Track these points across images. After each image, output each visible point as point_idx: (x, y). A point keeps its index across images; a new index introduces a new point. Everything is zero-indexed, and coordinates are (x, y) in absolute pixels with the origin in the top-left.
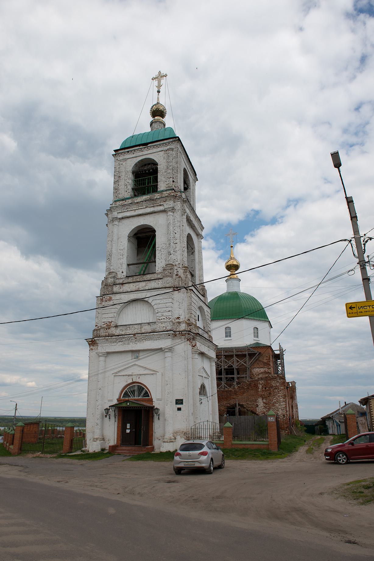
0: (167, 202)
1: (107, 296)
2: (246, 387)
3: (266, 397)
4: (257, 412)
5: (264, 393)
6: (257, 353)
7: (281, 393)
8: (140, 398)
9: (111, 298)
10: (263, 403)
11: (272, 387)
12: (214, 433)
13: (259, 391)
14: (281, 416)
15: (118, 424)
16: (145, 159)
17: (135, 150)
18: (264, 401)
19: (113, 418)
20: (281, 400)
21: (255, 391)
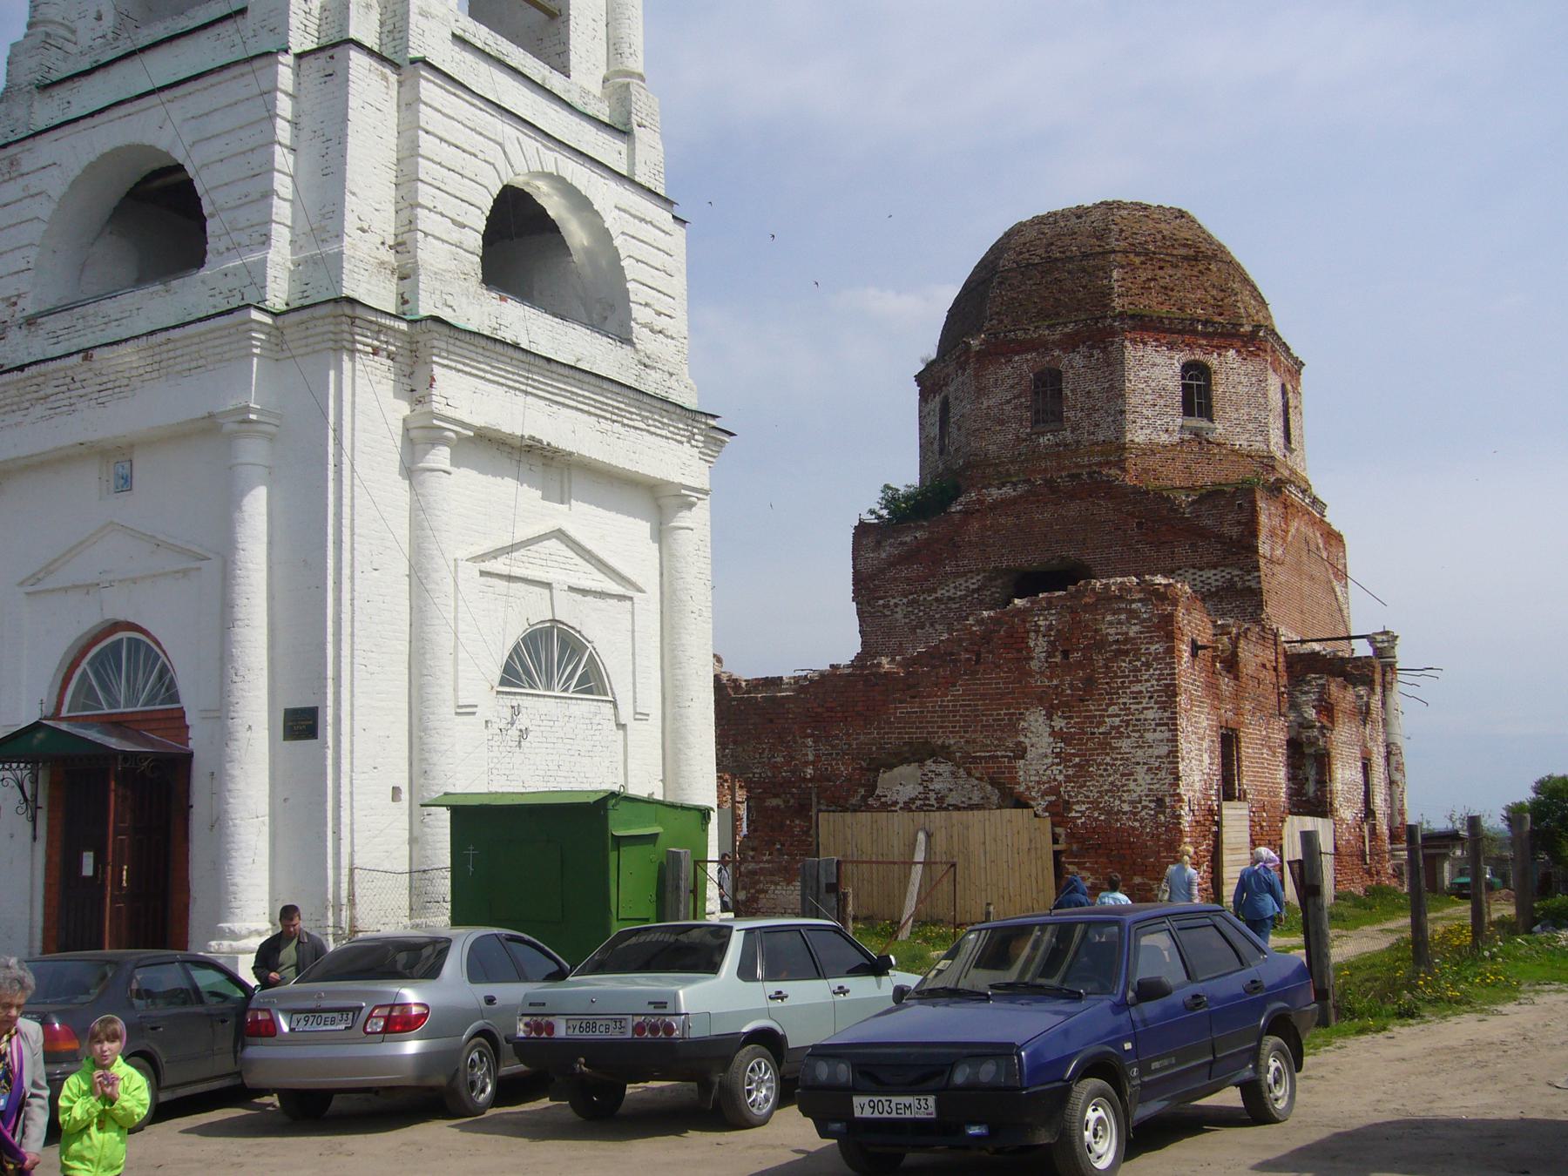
2: (966, 650)
3: (1067, 704)
4: (1019, 784)
5: (1055, 682)
7: (1151, 676)
8: (139, 708)
10: (1053, 733)
11: (1101, 644)
13: (1030, 674)
14: (1145, 807)
18: (1059, 723)
20: (1150, 714)
21: (1010, 669)
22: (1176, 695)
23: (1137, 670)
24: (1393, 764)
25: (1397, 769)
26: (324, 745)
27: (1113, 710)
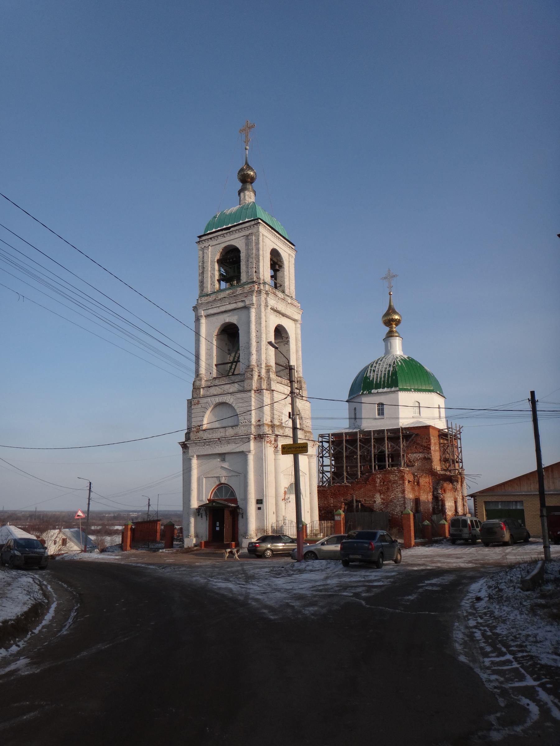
0: (249, 298)
1: (195, 399)
5: (381, 488)
6: (412, 435)
9: (199, 401)
10: (381, 498)
11: (390, 481)
12: (311, 531)
13: (376, 486)
15: (209, 523)
16: (229, 245)
17: (217, 236)
18: (382, 496)
19: (204, 517)
22: (405, 491)
23: (397, 486)
24: (464, 501)
25: (465, 502)
26: (264, 505)
27: (393, 494)
